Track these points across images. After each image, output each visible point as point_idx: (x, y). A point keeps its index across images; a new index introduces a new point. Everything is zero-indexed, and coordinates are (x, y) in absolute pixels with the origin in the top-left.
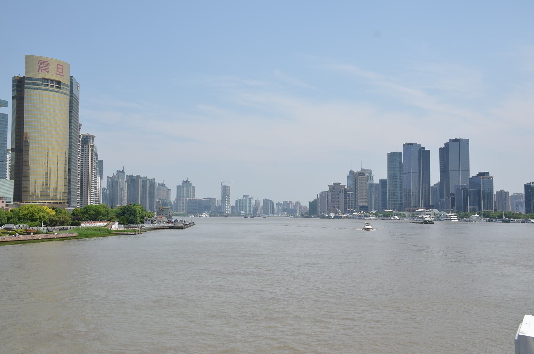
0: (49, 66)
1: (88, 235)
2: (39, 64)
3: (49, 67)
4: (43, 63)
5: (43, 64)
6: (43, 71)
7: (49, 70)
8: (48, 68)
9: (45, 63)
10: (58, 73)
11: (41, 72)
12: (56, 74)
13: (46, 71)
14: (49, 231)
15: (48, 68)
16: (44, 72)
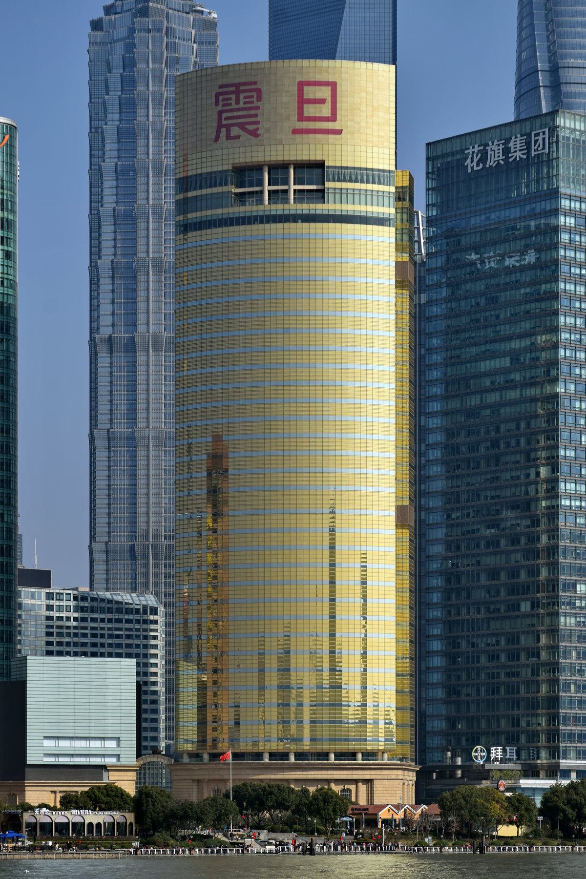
0: (259, 104)
1: (140, 778)
2: (217, 103)
3: (258, 108)
4: (233, 96)
5: (233, 102)
6: (235, 131)
7: (257, 123)
8: (253, 112)
9: (244, 91)
10: (253, 87)
11: (229, 137)
12: (295, 132)
13: (245, 130)
14: (239, 831)
15: (253, 112)
16: (238, 137)
